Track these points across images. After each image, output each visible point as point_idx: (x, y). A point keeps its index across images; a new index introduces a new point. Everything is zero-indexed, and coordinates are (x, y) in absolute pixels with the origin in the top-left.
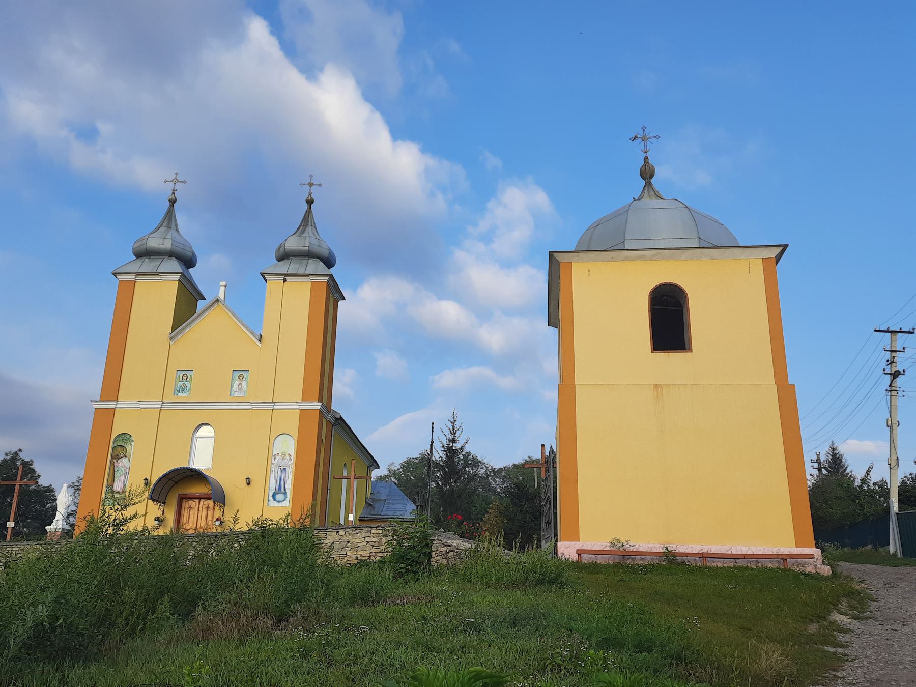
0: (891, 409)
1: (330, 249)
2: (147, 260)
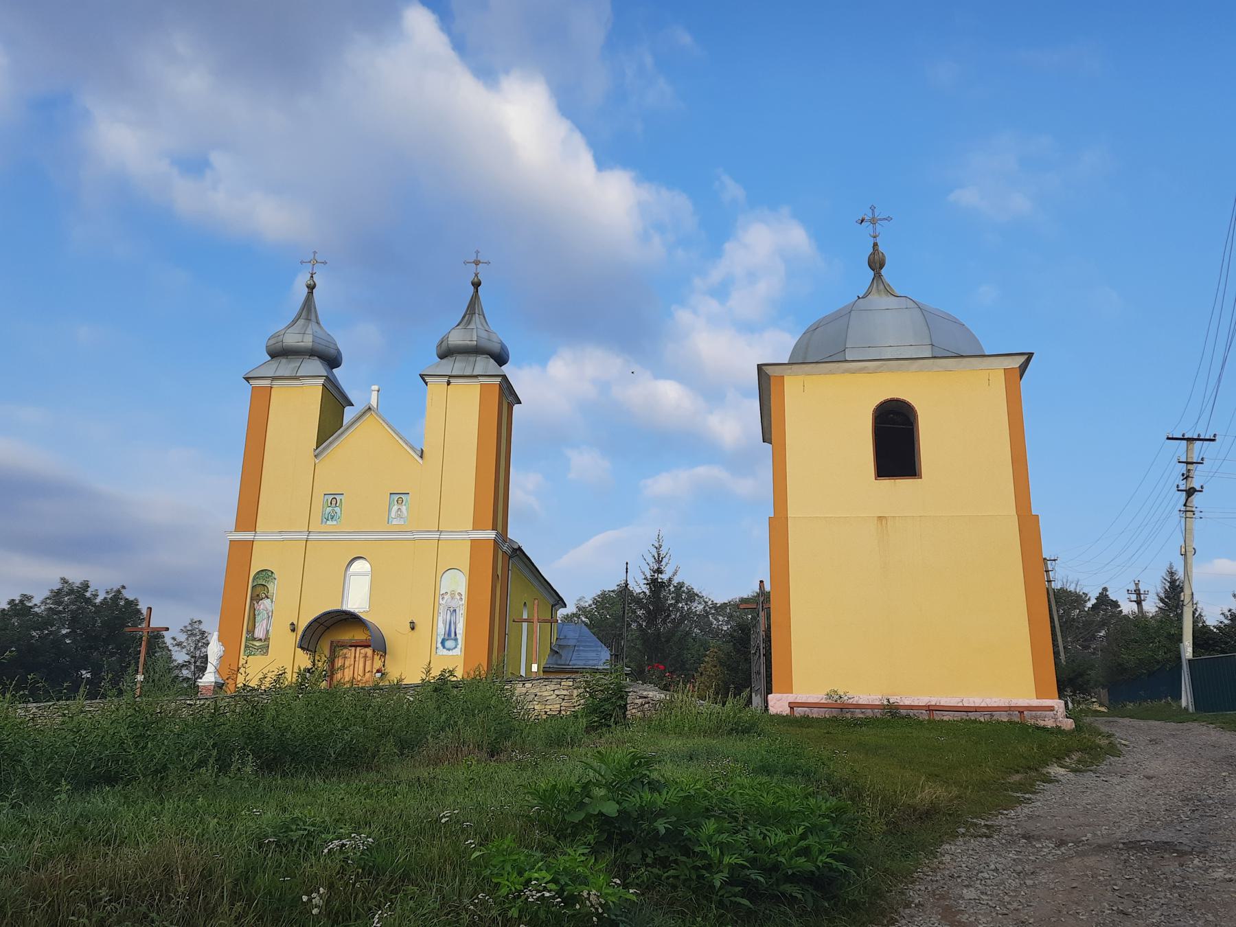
0: (1187, 533)
1: (502, 343)
2: (284, 361)
